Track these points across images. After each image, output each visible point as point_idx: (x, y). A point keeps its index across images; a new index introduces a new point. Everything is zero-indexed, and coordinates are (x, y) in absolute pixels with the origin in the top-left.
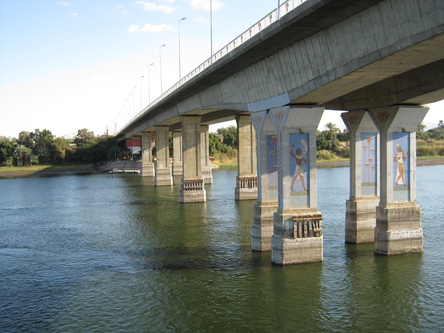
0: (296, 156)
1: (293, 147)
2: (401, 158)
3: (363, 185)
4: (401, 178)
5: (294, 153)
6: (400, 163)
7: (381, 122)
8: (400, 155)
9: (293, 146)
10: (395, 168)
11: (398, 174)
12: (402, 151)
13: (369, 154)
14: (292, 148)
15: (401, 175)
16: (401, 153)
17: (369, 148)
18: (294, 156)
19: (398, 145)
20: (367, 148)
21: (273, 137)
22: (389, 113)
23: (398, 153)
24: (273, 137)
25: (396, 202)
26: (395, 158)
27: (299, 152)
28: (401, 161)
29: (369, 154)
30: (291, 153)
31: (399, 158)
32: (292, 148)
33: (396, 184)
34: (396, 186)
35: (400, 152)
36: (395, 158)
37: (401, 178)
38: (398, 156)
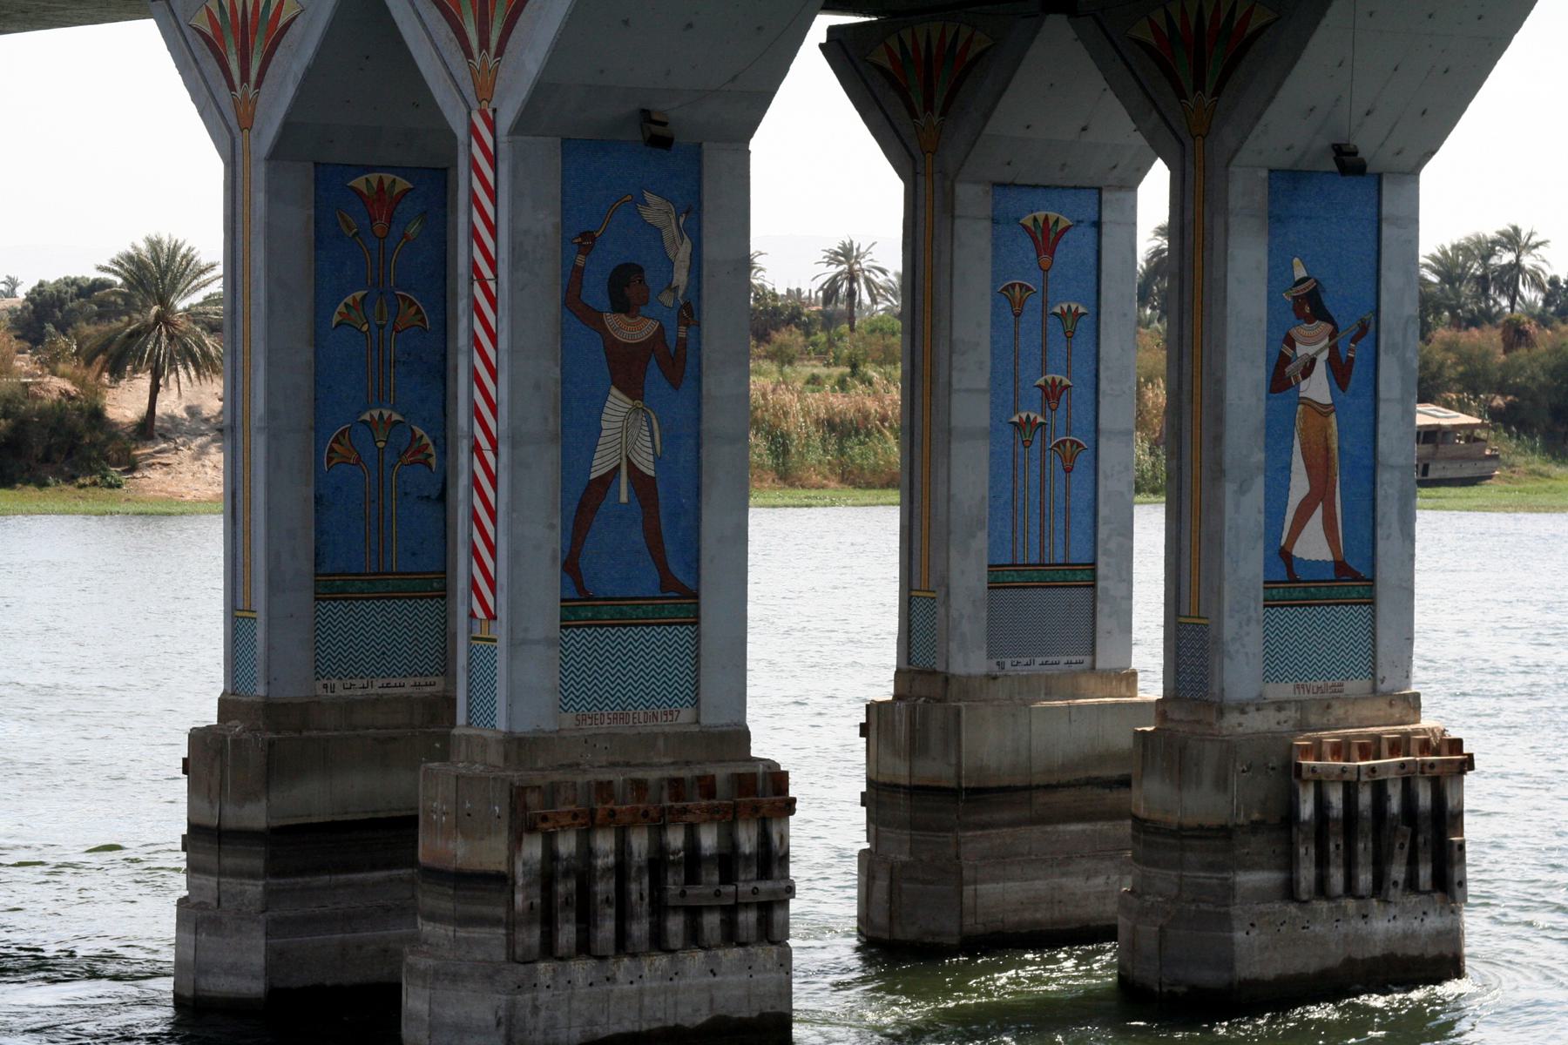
0: (611, 320)
1: (585, 250)
2: (1321, 368)
3: (1002, 577)
4: (1319, 513)
5: (596, 293)
6: (1309, 403)
7: (1180, 93)
8: (1312, 344)
9: (587, 241)
10: (1276, 436)
11: (1300, 486)
12: (1328, 318)
13: (1044, 348)
14: (581, 260)
15: (1320, 493)
16: (1323, 327)
17: (1045, 303)
18: (591, 318)
19: (1300, 272)
20: (1034, 302)
21: (359, 183)
22: (976, 48)
23: (1302, 330)
24: (359, 183)
25: (1285, 690)
26: (1283, 361)
27: (626, 288)
28: (1317, 388)
29: (1044, 348)
30: (573, 301)
31: (1307, 371)
32: (581, 260)
33: (1286, 555)
34: (1282, 574)
35: (1309, 319)
36: (1283, 361)
37: (1319, 513)
38: (1302, 350)
